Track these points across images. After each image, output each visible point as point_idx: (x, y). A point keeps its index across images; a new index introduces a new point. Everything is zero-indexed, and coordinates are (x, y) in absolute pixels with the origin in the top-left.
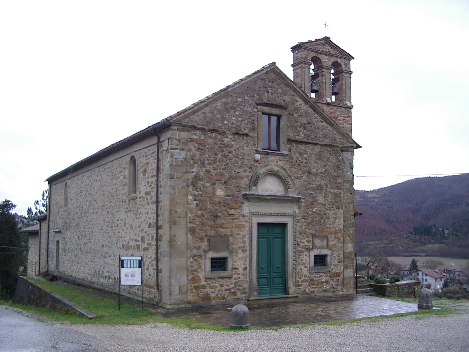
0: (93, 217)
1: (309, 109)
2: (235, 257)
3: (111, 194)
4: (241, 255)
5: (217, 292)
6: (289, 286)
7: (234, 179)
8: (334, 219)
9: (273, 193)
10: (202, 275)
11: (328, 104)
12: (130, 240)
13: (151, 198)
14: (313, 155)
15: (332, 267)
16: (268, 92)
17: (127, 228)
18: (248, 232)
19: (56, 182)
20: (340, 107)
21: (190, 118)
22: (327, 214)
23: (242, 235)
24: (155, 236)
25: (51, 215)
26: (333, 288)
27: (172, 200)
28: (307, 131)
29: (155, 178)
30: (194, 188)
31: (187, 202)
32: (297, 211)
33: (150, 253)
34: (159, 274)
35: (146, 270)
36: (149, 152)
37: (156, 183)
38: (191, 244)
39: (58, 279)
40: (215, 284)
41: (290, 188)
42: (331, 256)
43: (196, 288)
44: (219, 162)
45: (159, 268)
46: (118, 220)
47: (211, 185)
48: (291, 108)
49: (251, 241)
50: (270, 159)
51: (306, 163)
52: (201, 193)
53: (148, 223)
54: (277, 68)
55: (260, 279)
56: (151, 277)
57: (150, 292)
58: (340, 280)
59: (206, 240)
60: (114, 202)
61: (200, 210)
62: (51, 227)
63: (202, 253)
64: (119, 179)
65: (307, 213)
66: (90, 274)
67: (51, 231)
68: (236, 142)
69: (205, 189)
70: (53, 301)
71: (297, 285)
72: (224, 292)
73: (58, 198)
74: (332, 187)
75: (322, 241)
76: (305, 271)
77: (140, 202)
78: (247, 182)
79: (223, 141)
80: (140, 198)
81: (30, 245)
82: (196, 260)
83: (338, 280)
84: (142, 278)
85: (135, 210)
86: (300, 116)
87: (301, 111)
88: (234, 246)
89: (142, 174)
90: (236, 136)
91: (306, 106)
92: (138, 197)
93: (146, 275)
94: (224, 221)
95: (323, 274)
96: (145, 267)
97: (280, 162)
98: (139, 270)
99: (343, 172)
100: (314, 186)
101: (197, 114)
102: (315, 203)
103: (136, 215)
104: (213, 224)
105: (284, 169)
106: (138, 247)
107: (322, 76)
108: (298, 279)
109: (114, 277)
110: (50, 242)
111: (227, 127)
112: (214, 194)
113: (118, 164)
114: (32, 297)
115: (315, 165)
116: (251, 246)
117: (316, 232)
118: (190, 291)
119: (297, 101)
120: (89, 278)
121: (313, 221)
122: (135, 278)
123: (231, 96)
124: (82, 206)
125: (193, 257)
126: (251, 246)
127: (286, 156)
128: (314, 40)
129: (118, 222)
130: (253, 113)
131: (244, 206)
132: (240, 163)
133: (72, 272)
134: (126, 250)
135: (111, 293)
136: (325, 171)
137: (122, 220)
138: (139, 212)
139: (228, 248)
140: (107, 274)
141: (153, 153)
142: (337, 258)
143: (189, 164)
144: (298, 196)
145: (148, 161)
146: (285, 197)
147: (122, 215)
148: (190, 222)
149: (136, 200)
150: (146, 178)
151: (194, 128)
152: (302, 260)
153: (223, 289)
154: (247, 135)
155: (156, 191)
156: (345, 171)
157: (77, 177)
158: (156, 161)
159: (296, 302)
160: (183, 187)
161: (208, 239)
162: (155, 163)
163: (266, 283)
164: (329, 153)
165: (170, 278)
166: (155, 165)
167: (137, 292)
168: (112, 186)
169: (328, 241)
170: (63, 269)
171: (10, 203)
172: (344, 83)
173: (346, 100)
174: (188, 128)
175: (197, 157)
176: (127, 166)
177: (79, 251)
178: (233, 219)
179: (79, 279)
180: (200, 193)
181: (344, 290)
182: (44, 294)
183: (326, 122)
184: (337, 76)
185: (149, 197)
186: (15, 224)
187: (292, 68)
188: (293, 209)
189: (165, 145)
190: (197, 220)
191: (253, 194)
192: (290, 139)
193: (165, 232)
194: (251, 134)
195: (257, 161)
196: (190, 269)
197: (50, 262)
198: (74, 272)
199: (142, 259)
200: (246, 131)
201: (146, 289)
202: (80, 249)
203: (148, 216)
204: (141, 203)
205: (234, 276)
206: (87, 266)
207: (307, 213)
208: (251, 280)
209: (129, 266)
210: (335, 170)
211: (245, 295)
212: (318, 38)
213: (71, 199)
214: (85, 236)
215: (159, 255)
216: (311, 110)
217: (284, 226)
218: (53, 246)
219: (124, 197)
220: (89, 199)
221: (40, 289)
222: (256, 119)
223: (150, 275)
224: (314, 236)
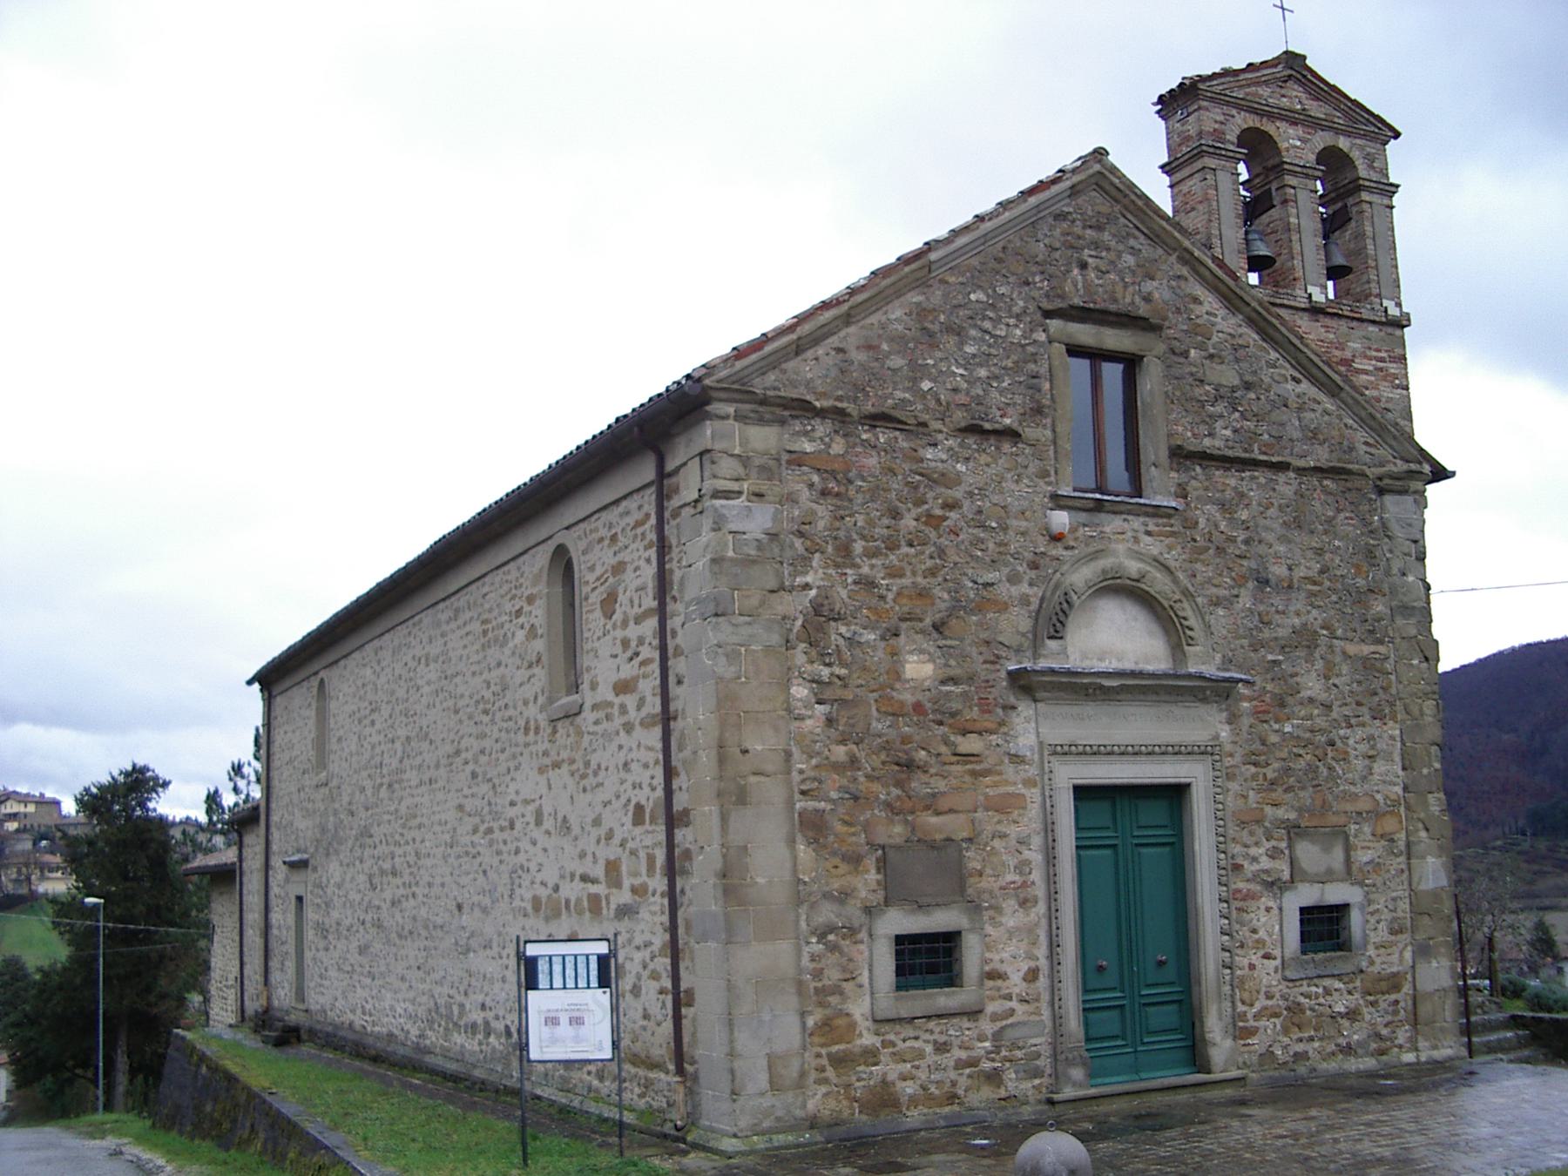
0: (418, 799)
1: (1245, 330)
2: (989, 929)
3: (481, 706)
4: (1012, 917)
5: (923, 1075)
6: (1209, 1036)
7: (972, 612)
8: (1367, 762)
9: (1128, 665)
10: (859, 1009)
11: (1315, 311)
12: (562, 877)
13: (641, 703)
14: (1272, 512)
15: (1371, 952)
16: (1083, 266)
17: (548, 833)
18: (1037, 825)
19: (288, 683)
20: (1361, 320)
21: (784, 372)
22: (1339, 744)
24: (660, 856)
25: (273, 805)
26: (1378, 1036)
27: (726, 701)
28: (1244, 417)
29: (652, 623)
30: (814, 653)
31: (789, 710)
32: (1225, 733)
33: (642, 926)
34: (684, 1010)
35: (628, 995)
36: (623, 524)
37: (656, 642)
38: (812, 880)
39: (304, 1036)
40: (916, 1044)
41: (1191, 641)
42: (1362, 908)
43: (839, 1061)
44: (911, 545)
45: (683, 986)
46: (512, 804)
47: (883, 638)
48: (1176, 326)
49: (1051, 858)
50: (1107, 529)
51: (1247, 542)
52: (843, 672)
53: (631, 807)
54: (1114, 170)
55: (1091, 1015)
56: (651, 1024)
57: (648, 1085)
58: (1402, 1004)
59: (870, 862)
60: (496, 735)
61: (843, 742)
62: (274, 847)
63: (858, 918)
64: (511, 645)
65: (1264, 743)
66: (413, 1018)
67: (276, 862)
68: (971, 464)
69: (857, 652)
70: (272, 1126)
71: (1242, 1033)
72: (953, 1075)
73: (296, 738)
74: (1350, 634)
75: (1327, 849)
76: (1267, 974)
77: (596, 723)
78: (1025, 624)
79: (922, 461)
80: (595, 707)
81: (215, 919)
82: (833, 948)
83: (1396, 1002)
84: (616, 1029)
85: (578, 756)
86: (1211, 356)
87: (1215, 339)
88: (985, 883)
89: (598, 613)
90: (970, 440)
91: (1233, 321)
92: (587, 706)
93: (631, 1013)
94: (941, 785)
95: (1338, 985)
96: (626, 984)
97: (1148, 539)
98: (603, 998)
99: (1388, 573)
100: (1281, 632)
101: (810, 354)
102: (1290, 700)
103: (584, 777)
104: (898, 797)
105: (1167, 569)
106: (595, 903)
107: (1285, 202)
108: (1241, 1008)
109: (507, 1027)
110: (273, 901)
111: (932, 404)
112: (897, 675)
113: (506, 587)
114: (208, 1108)
115: (1282, 549)
116: (1051, 879)
117: (1301, 816)
118: (813, 1075)
119: (1196, 300)
120: (414, 1032)
121: (1287, 771)
122: (583, 1030)
123: (943, 282)
124: (378, 759)
125: (822, 937)
126: (1051, 879)
127: (1169, 516)
128: (1243, 66)
129: (512, 812)
130: (1030, 349)
131: (1017, 720)
132: (991, 545)
133: (353, 1011)
134: (547, 919)
135: (497, 1091)
136: (1322, 572)
137: (526, 802)
138: (593, 765)
139: (962, 889)
140: (477, 1016)
141: (638, 524)
142: (1386, 915)
143: (788, 553)
144: (1227, 675)
145: (620, 557)
146: (1176, 676)
147: (528, 783)
148: (803, 793)
149: (579, 719)
150: (614, 627)
151: (803, 408)
152: (1254, 931)
153: (948, 1060)
154: (1012, 435)
155: (657, 673)
156: (1395, 571)
157: (356, 655)
158: (653, 553)
159: (1243, 1103)
160: (768, 649)
161: (878, 860)
162: (648, 561)
163: (1116, 1030)
164: (1330, 499)
165: (730, 1024)
166: (650, 571)
167: (596, 1083)
168: (485, 675)
169: (1348, 849)
170: (322, 1000)
171: (150, 774)
172: (1368, 229)
173: (1379, 296)
174: (778, 411)
175: (821, 524)
176: (542, 588)
177: (373, 931)
178: (975, 774)
179: (378, 1037)
180: (838, 671)
181: (1422, 1044)
182: (243, 1098)
183: (1313, 380)
184: (1339, 205)
185: (630, 701)
186: (165, 846)
187: (1166, 180)
188: (1204, 724)
189: (689, 486)
190: (833, 786)
191: (1052, 671)
192: (1179, 447)
193: (703, 839)
194: (1029, 432)
195: (1057, 538)
196: (813, 985)
197: (275, 976)
198: (359, 1012)
199: (613, 952)
200: (1008, 421)
201: (633, 1070)
202: (378, 925)
203: (630, 778)
204: (598, 729)
205: (991, 1008)
206: (405, 986)
207: (1264, 743)
208: (1057, 1019)
209: (558, 983)
210: (1357, 567)
211: (1037, 1082)
212: (1257, 60)
213: (340, 739)
214: (394, 874)
215: (681, 931)
216: (1252, 336)
217: (1177, 793)
218: (282, 917)
219: (532, 711)
220: (402, 732)
221: (231, 1079)
222: (1044, 370)
223: (646, 1016)
224: (1294, 831)
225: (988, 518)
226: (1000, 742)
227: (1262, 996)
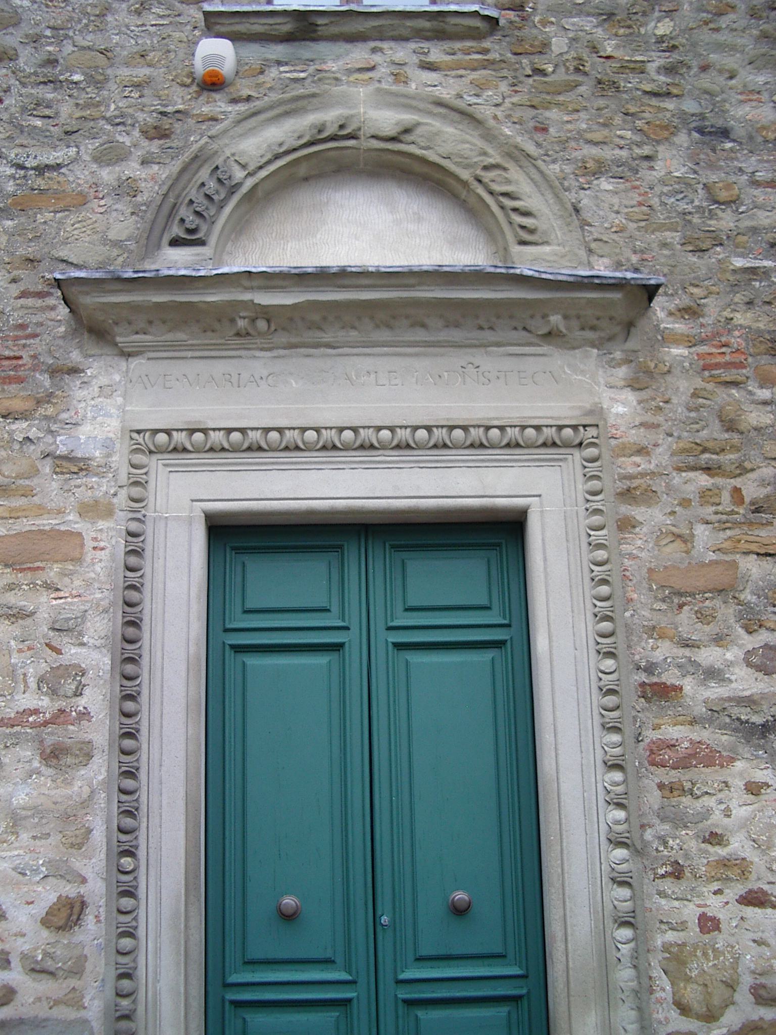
23: (43, 615)
65: (730, 426)
131: (81, 394)
188: (583, 385)
195: (213, 84)
207: (730, 426)
217: (500, 533)
225: (70, 69)
226: (33, 433)
227: (743, 996)
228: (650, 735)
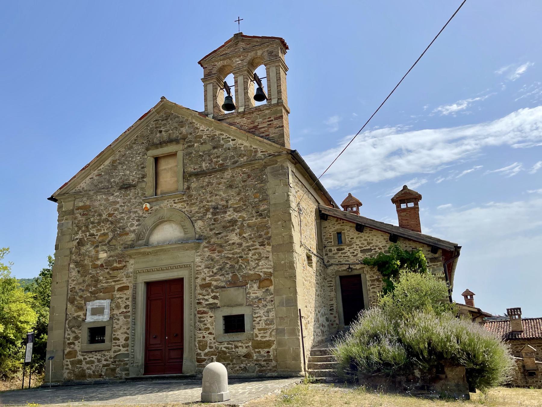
228: (198, 310)
